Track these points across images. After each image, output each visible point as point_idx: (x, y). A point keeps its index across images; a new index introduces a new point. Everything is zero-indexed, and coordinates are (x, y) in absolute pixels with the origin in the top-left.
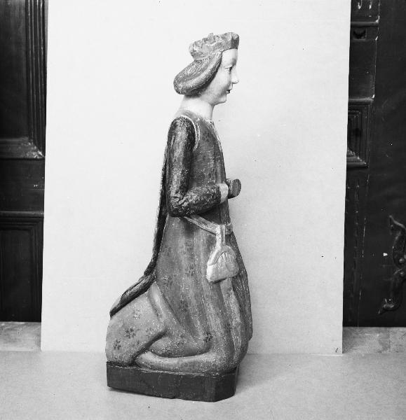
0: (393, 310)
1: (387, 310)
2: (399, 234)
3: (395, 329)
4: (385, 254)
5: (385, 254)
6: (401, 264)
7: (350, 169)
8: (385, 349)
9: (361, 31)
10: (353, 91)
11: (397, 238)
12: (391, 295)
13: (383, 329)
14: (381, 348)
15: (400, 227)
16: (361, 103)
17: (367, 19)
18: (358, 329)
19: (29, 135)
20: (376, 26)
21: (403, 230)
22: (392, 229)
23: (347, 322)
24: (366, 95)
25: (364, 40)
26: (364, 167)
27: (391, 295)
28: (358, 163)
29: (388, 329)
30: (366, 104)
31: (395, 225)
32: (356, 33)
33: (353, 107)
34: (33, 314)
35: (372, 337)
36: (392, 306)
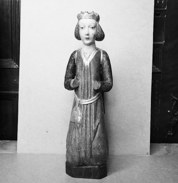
0: (173, 135)
1: (169, 136)
2: (175, 102)
3: (173, 144)
4: (169, 111)
5: (169, 111)
9: (159, 13)
11: (174, 104)
13: (168, 144)
14: (167, 152)
17: (161, 7)
18: (157, 144)
20: (165, 11)
21: (177, 101)
22: (172, 100)
23: (152, 142)
24: (161, 41)
30: (161, 45)
31: (173, 99)
32: (156, 13)
33: (155, 47)
35: (163, 148)
36: (172, 134)
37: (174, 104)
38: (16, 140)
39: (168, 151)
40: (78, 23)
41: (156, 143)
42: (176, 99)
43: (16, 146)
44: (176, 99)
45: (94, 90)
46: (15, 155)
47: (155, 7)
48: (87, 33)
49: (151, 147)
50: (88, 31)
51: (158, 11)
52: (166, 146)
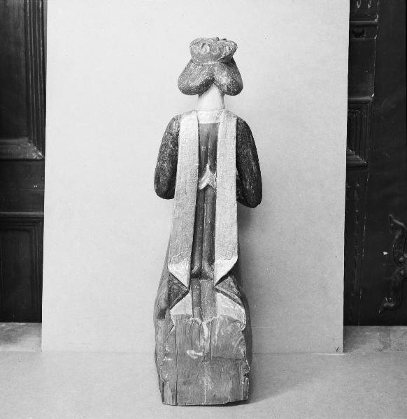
1: (387, 308)
3: (395, 328)
4: (385, 253)
5: (385, 253)
6: (401, 263)
7: (350, 168)
8: (385, 348)
10: (352, 91)
11: (397, 237)
12: (392, 293)
13: (383, 327)
15: (400, 226)
16: (361, 102)
17: (366, 18)
18: (358, 328)
19: (28, 135)
20: (375, 25)
24: (365, 94)
25: (364, 39)
26: (364, 166)
27: (392, 293)
28: (357, 162)
29: (389, 327)
30: (366, 102)
31: (395, 224)
32: (355, 32)
33: (353, 107)
34: (33, 315)
35: (373, 336)
37: (397, 237)
38: (41, 322)
41: (356, 324)
42: (402, 224)
44: (402, 224)
51: (359, 26)
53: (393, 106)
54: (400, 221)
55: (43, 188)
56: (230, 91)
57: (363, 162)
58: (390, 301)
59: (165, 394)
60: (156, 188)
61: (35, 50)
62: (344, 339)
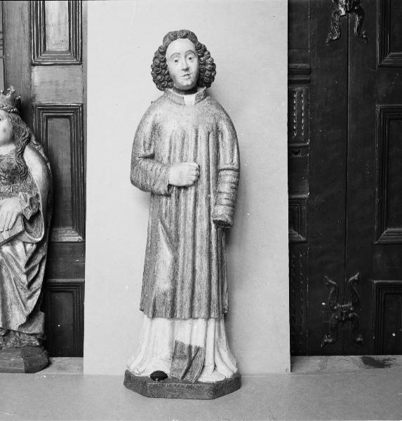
0: (332, 343)
1: (327, 343)
3: (333, 357)
4: (323, 304)
5: (323, 304)
7: (293, 245)
9: (297, 150)
11: (331, 292)
13: (324, 357)
14: (319, 368)
17: (301, 142)
18: (305, 357)
20: (308, 146)
24: (302, 193)
30: (304, 199)
31: (329, 283)
33: (292, 203)
35: (314, 362)
36: (331, 341)
37: (331, 292)
38: (81, 355)
39: (323, 367)
40: (173, 337)
41: (305, 355)
42: (334, 283)
43: (81, 365)
44: (334, 283)
45: (385, 360)
46: (79, 377)
47: (289, 142)
48: (185, 68)
49: (292, 363)
50: (182, 67)
52: (321, 359)
53: (323, 201)
54: (333, 281)
55: (84, 262)
56: (202, 72)
57: (303, 239)
58: (328, 338)
59: (190, 332)
60: (4, 285)
61: (78, 168)
62: (291, 363)
